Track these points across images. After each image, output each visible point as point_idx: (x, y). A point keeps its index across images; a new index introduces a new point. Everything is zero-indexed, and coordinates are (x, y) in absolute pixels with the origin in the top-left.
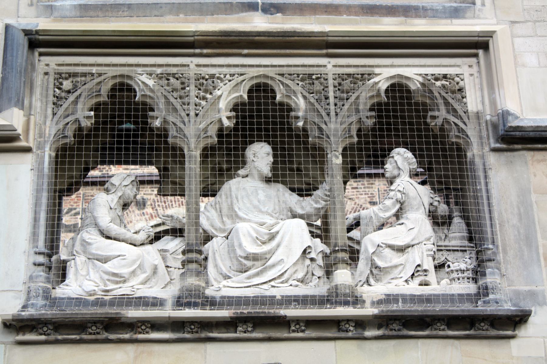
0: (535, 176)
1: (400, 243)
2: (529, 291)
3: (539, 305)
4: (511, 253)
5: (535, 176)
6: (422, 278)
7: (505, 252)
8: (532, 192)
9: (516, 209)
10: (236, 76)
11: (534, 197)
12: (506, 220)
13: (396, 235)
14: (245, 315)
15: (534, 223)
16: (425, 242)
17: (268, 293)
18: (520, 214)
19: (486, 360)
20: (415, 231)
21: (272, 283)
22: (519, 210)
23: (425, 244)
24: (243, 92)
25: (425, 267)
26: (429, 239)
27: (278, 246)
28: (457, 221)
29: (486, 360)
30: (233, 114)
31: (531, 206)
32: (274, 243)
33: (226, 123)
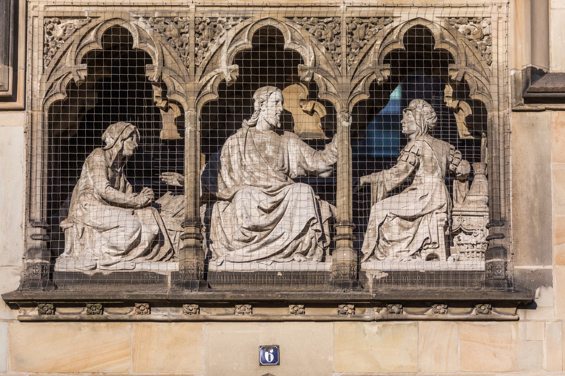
0: (557, 141)
1: (411, 214)
2: (536, 271)
3: (545, 286)
4: (522, 229)
5: (557, 141)
6: (429, 251)
7: (516, 228)
8: (552, 160)
9: (532, 180)
10: (240, 19)
11: (553, 166)
12: (520, 193)
13: (408, 203)
14: (243, 299)
15: (550, 196)
16: (437, 211)
17: (270, 268)
18: (536, 186)
19: (484, 344)
20: (428, 199)
21: (273, 258)
22: (536, 180)
23: (437, 213)
24: (248, 39)
25: (434, 239)
26: (441, 207)
27: (282, 215)
28: (480, 180)
29: (484, 344)
30: (236, 67)
31: (549, 176)
32: (279, 211)
33: (228, 79)
